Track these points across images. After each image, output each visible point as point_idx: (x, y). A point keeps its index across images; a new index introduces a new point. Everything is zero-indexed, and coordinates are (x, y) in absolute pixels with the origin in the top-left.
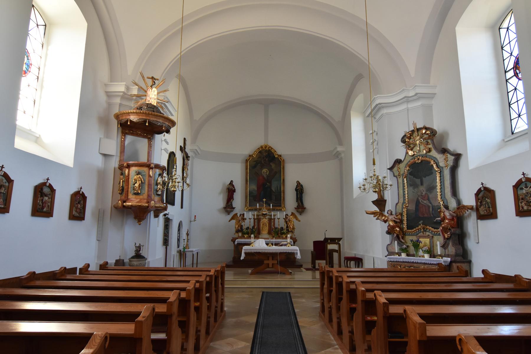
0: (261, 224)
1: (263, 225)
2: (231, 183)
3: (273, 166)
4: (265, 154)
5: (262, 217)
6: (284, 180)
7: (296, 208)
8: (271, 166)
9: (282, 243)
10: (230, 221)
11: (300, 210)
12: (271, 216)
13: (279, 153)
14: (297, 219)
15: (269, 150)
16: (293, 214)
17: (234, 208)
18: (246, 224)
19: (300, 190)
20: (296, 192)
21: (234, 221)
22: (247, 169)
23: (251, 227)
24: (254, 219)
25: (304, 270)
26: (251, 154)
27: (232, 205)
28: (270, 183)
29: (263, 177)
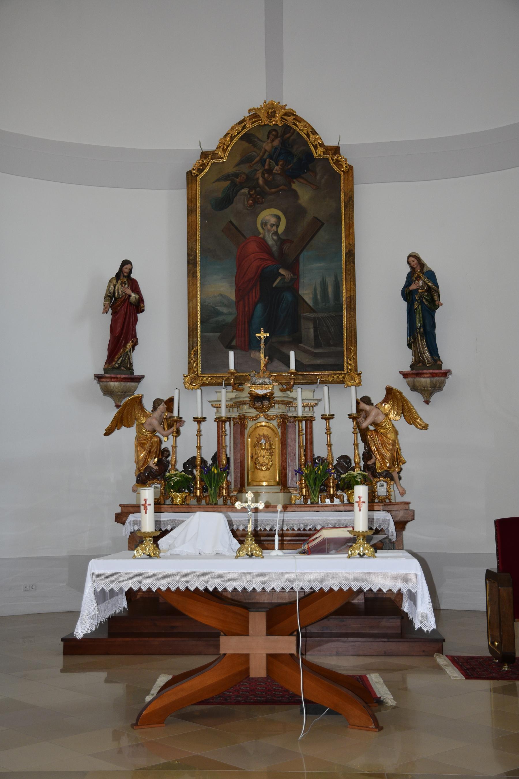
2: (124, 274)
3: (304, 194)
4: (267, 146)
5: (249, 411)
6: (351, 254)
9: (326, 534)
10: (108, 432)
11: (425, 381)
12: (289, 404)
14: (410, 417)
15: (287, 128)
16: (391, 394)
17: (139, 379)
18: (184, 448)
19: (421, 296)
20: (404, 305)
21: (127, 435)
22: (191, 211)
23: (208, 455)
24: (219, 421)
25: (454, 673)
26: (211, 146)
27: (130, 369)
28: (294, 267)
29: (263, 244)
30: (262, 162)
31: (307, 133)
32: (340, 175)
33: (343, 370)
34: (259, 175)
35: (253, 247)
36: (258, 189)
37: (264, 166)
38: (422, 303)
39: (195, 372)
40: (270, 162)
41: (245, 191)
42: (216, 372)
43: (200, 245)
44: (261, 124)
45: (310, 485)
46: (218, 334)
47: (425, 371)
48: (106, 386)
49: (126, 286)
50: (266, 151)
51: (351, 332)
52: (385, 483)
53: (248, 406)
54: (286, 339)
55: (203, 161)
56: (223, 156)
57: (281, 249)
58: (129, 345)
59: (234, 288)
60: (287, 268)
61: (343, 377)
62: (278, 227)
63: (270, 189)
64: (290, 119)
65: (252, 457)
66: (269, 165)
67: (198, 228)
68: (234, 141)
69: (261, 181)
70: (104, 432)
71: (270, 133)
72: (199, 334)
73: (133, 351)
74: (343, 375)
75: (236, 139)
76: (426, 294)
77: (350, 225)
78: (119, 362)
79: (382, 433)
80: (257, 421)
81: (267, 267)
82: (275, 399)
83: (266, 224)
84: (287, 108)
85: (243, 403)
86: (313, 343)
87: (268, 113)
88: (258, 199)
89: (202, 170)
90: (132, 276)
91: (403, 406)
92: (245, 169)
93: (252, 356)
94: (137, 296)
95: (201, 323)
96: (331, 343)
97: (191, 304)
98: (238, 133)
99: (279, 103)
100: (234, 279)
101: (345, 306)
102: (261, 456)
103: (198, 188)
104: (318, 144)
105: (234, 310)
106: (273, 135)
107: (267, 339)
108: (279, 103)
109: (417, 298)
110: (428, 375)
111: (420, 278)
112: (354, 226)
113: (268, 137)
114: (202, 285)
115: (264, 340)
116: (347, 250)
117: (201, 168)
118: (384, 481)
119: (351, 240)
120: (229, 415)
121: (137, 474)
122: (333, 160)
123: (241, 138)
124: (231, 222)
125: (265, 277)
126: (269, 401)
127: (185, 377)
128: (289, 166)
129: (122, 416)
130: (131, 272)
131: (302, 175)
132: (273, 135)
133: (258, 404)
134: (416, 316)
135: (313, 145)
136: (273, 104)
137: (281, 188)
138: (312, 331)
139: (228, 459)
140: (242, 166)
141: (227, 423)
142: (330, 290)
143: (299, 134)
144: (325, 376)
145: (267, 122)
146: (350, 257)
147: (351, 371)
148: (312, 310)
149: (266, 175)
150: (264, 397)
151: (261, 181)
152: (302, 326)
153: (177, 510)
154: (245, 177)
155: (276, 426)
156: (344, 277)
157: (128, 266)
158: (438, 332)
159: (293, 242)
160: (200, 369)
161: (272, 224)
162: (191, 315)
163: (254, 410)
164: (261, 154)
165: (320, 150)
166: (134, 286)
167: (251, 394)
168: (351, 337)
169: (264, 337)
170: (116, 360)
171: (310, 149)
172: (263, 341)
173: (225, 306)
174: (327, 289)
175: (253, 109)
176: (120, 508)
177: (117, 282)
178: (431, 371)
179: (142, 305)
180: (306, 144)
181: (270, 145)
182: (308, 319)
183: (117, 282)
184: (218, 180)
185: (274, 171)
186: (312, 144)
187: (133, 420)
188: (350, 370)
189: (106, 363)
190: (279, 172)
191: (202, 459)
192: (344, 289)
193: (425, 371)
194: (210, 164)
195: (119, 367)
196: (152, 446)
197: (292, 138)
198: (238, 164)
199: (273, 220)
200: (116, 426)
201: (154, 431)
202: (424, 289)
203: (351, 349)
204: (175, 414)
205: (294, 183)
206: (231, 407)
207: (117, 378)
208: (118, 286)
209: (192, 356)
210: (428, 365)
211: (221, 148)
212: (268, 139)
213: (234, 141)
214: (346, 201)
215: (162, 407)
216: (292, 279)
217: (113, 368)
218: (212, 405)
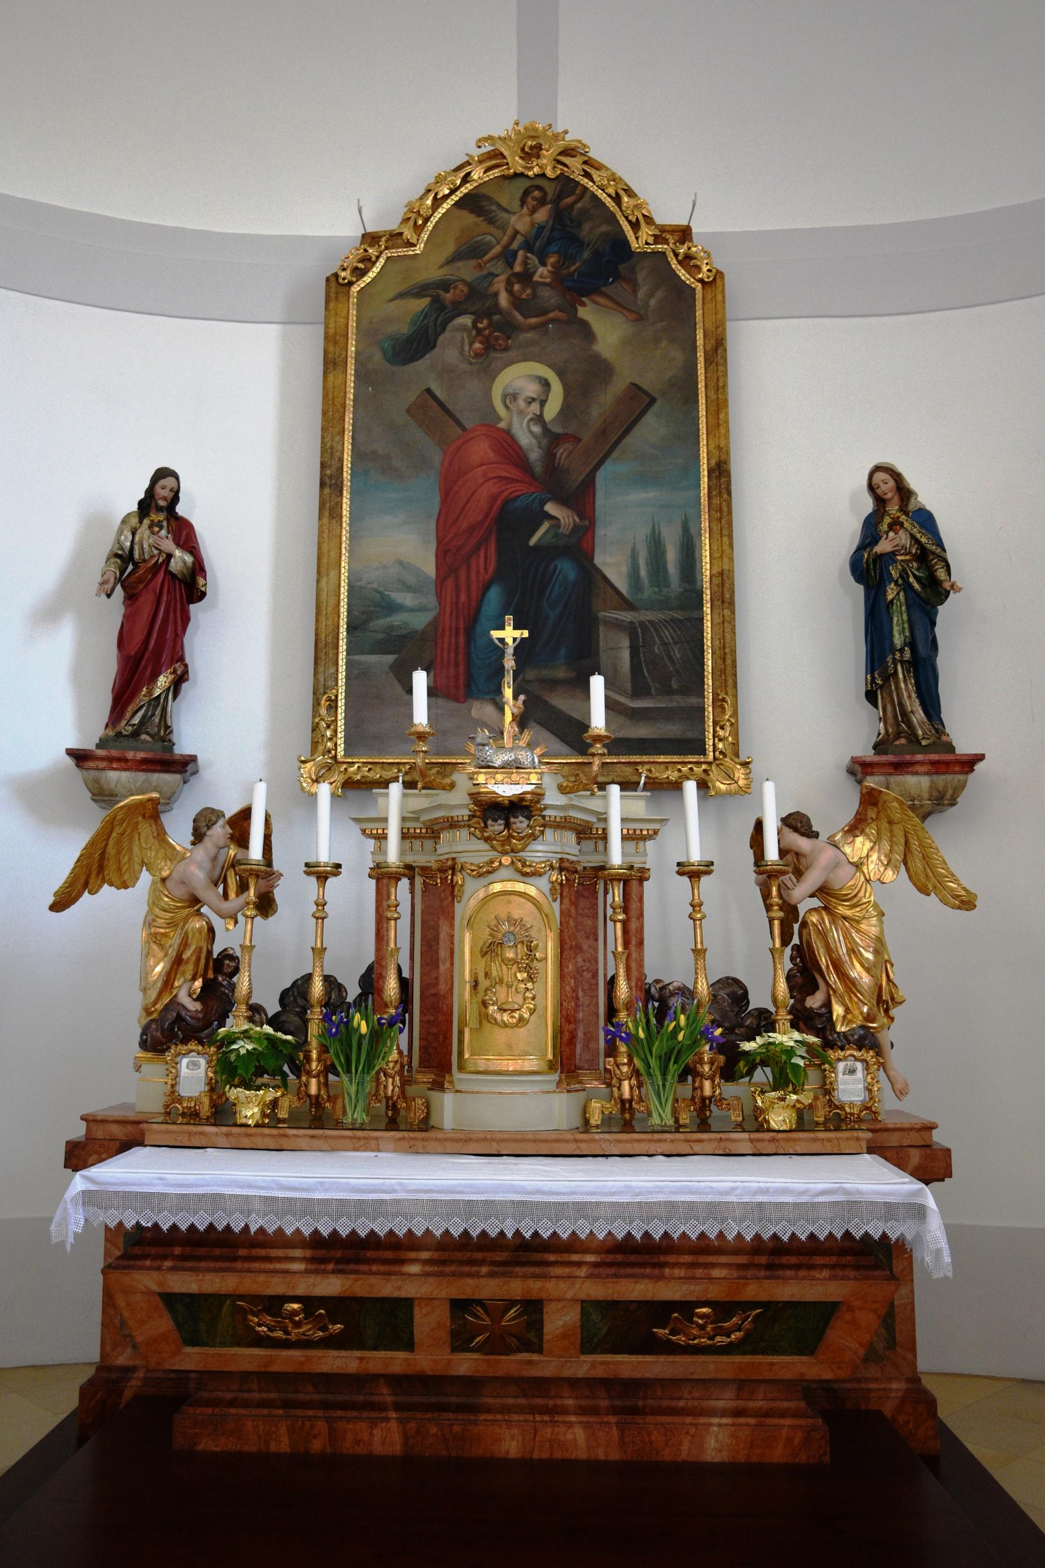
0: (466, 945)
1: (490, 950)
2: (161, 501)
3: (608, 330)
4: (521, 222)
5: (465, 847)
6: (721, 472)
7: (79, 757)
8: (586, 332)
10: (62, 902)
12: (592, 833)
13: (668, 213)
15: (565, 183)
17: (970, 763)
18: (273, 954)
19: (900, 574)
21: (120, 910)
22: (332, 363)
27: (164, 735)
28: (581, 499)
29: (506, 445)
30: (508, 257)
31: (617, 193)
32: (694, 289)
33: (704, 752)
34: (499, 284)
35: (481, 450)
36: (496, 318)
37: (511, 265)
38: (907, 587)
39: (329, 752)
40: (527, 258)
41: (466, 320)
42: (381, 752)
43: (353, 445)
44: (506, 173)
45: (650, 1075)
46: (390, 658)
47: (919, 757)
48: (97, 781)
49: (163, 532)
50: (516, 232)
51: (724, 660)
52: (859, 1066)
53: (464, 832)
54: (561, 673)
55: (366, 250)
56: (414, 241)
57: (549, 455)
58: (163, 681)
59: (433, 547)
60: (563, 500)
61: (705, 771)
62: (543, 403)
63: (525, 317)
64: (575, 164)
65: (475, 985)
66: (525, 263)
67: (350, 403)
68: (442, 211)
69: (504, 300)
70: (51, 900)
71: (526, 193)
72: (342, 656)
73: (175, 697)
74: (704, 767)
75: (446, 206)
76: (915, 565)
77: (719, 406)
78: (136, 720)
79: (845, 918)
80: (491, 878)
81: (518, 497)
82: (546, 813)
83: (514, 397)
84: (568, 137)
85: (453, 824)
86: (628, 685)
87: (523, 150)
88: (497, 339)
89: (363, 273)
90: (180, 509)
91: (907, 842)
92: (467, 271)
93: (474, 713)
94: (189, 559)
95: (348, 630)
96: (675, 685)
97: (324, 580)
98: (453, 192)
99: (550, 126)
100: (432, 525)
101: (707, 597)
102: (501, 981)
103: (353, 312)
104: (641, 218)
105: (431, 601)
106: (534, 199)
107: (521, 646)
108: (550, 126)
109: (895, 574)
110: (925, 768)
111: (902, 525)
112: (727, 406)
113: (523, 202)
114: (352, 538)
115: (515, 649)
116: (713, 462)
117: (361, 265)
118: (856, 1059)
119: (722, 439)
120: (410, 859)
121: (144, 1022)
122: (676, 255)
123: (457, 205)
124: (429, 391)
125: (511, 522)
126: (529, 818)
127: (304, 762)
128: (573, 268)
129: (103, 855)
130: (175, 499)
131: (603, 289)
132: (534, 199)
133: (497, 827)
134: (891, 619)
135: (629, 222)
136: (536, 130)
137: (551, 315)
138: (626, 655)
139: (405, 985)
140: (460, 264)
141: (404, 883)
142: (672, 556)
143: (595, 197)
144: (658, 766)
145: (520, 170)
146: (719, 477)
147: (725, 756)
148: (628, 605)
149: (517, 287)
150: (517, 807)
151: (504, 300)
152: (602, 643)
153: (246, 1142)
154: (466, 290)
155: (547, 893)
156: (705, 524)
157: (169, 482)
158: (943, 662)
159: (579, 440)
160: (341, 741)
161: (529, 397)
162: (323, 609)
163: (483, 846)
164: (506, 239)
165: (646, 232)
166: (184, 534)
167: (474, 796)
168: (723, 671)
169: (515, 639)
170: (128, 715)
171: (623, 231)
172: (510, 651)
173: (409, 589)
174: (664, 553)
175: (489, 139)
176: (84, 1123)
177: (141, 522)
178: (934, 757)
179: (201, 581)
180: (612, 218)
181: (527, 219)
182: (617, 625)
183: (141, 522)
184: (402, 295)
185: (536, 278)
186: (627, 218)
187: (137, 867)
188: (721, 752)
189: (107, 726)
190: (548, 280)
191: (330, 981)
192: (706, 554)
193: (919, 757)
194: (382, 261)
195: (135, 734)
196: (184, 944)
197: (579, 205)
198: (451, 261)
199: (532, 389)
200: (86, 885)
201: (195, 901)
202: (910, 553)
203: (724, 700)
204: (256, 851)
205: (584, 305)
206: (415, 838)
207: (126, 760)
208: (144, 531)
209: (323, 711)
210: (924, 743)
211: (411, 223)
212: (522, 206)
213: (442, 211)
214: (708, 349)
215: (219, 831)
216: (576, 528)
217: (119, 735)
218: (364, 831)
